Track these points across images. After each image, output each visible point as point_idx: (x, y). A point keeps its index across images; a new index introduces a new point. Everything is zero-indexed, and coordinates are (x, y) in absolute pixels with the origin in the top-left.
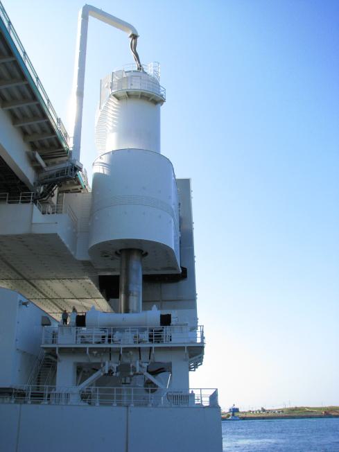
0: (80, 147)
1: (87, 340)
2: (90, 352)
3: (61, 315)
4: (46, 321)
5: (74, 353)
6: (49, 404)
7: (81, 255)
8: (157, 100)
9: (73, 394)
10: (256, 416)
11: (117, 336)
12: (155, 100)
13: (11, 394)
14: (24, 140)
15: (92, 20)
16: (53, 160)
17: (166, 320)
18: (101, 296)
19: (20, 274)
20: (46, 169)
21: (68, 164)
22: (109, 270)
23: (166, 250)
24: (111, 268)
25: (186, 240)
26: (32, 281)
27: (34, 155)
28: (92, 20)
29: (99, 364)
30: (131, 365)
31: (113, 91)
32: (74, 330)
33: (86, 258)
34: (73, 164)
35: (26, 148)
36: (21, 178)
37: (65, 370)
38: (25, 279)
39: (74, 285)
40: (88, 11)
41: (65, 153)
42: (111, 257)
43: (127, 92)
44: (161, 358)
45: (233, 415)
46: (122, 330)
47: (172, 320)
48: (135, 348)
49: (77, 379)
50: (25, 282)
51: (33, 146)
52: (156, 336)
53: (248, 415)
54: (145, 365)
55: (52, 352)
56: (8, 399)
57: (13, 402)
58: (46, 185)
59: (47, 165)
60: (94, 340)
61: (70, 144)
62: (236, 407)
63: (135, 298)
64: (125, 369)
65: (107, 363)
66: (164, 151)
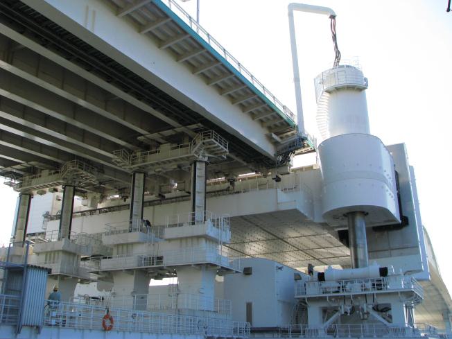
3: (306, 268)
4: (298, 277)
6: (305, 337)
7: (318, 219)
9: (321, 329)
11: (348, 287)
12: (357, 88)
13: (278, 331)
14: (262, 126)
15: (295, 13)
16: (285, 134)
17: (384, 272)
18: (342, 244)
19: (275, 236)
21: (296, 138)
22: (342, 227)
23: (385, 212)
24: (344, 225)
25: (404, 194)
26: (285, 240)
27: (271, 135)
28: (295, 13)
32: (317, 283)
33: (322, 221)
35: (267, 132)
37: (314, 313)
38: (279, 238)
39: (319, 240)
41: (295, 127)
44: (381, 301)
47: (389, 271)
49: (323, 318)
50: (280, 240)
51: (270, 128)
54: (371, 307)
59: (281, 138)
60: (331, 290)
61: (296, 122)
65: (342, 306)
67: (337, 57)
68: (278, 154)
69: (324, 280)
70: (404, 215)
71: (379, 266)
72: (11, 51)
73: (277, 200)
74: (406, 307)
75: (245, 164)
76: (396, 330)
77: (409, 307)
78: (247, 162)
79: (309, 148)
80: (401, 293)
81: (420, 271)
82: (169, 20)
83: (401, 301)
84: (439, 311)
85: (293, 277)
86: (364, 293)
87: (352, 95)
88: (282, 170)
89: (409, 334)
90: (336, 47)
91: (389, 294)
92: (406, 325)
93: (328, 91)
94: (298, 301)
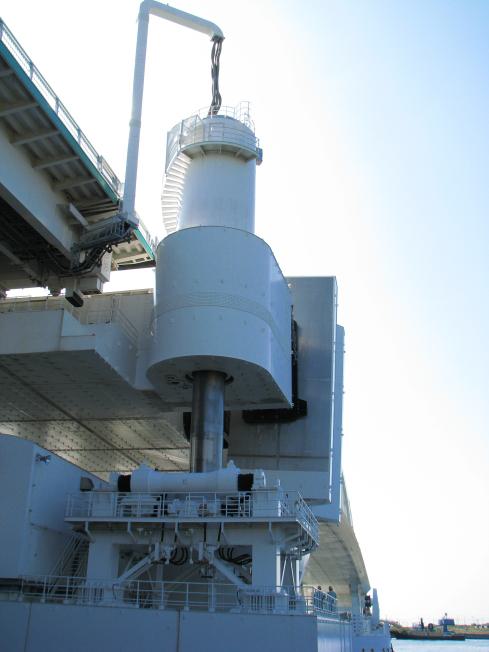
0: (134, 196)
2: (132, 529)
5: (112, 530)
7: (141, 383)
8: (248, 155)
10: (481, 633)
11: (172, 508)
13: (20, 587)
14: (53, 188)
17: (245, 482)
19: (65, 413)
20: (88, 228)
23: (260, 375)
27: (68, 207)
29: (147, 547)
30: (191, 550)
31: (183, 146)
34: (123, 219)
35: (61, 200)
36: (50, 241)
37: (101, 558)
40: (151, 6)
42: (182, 383)
43: (202, 147)
44: (234, 539)
45: (445, 630)
46: (180, 497)
47: (255, 481)
48: (197, 524)
51: (69, 196)
52: (230, 508)
53: (470, 632)
54: (212, 549)
55: (79, 528)
56: (16, 595)
57: (21, 599)
58: (90, 251)
59: (91, 223)
61: (121, 193)
62: (449, 617)
63: (211, 443)
64: (181, 557)
65: (157, 546)
66: (261, 229)
67: (214, 104)
68: (78, 248)
69: (129, 490)
70: (300, 397)
71: (239, 471)
73: (61, 329)
74: (283, 556)
75: (16, 260)
76: (256, 599)
77: (289, 558)
78: (21, 259)
79: (144, 256)
80: (275, 524)
81: (325, 501)
82: (56, 133)
83: (272, 543)
84: (346, 580)
85: (77, 486)
87: (230, 164)
88: (86, 284)
89: (282, 607)
90: (216, 86)
91: (251, 525)
92: (278, 590)
93: (185, 152)
94: (72, 527)
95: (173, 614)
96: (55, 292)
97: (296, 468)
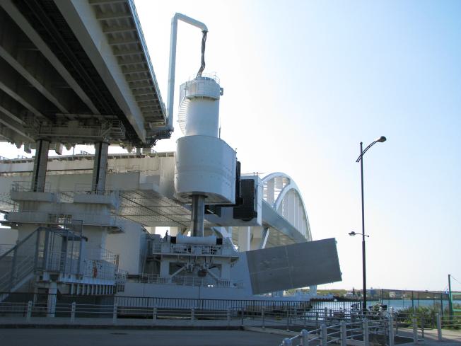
1: (177, 250)
11: (193, 249)
15: (179, 22)
28: (179, 22)
37: (165, 266)
44: (216, 262)
67: (202, 67)
72: (19, 43)
73: (139, 181)
86: (204, 255)
87: (209, 103)
95: (197, 288)
96: (129, 151)
97: (94, 179)
